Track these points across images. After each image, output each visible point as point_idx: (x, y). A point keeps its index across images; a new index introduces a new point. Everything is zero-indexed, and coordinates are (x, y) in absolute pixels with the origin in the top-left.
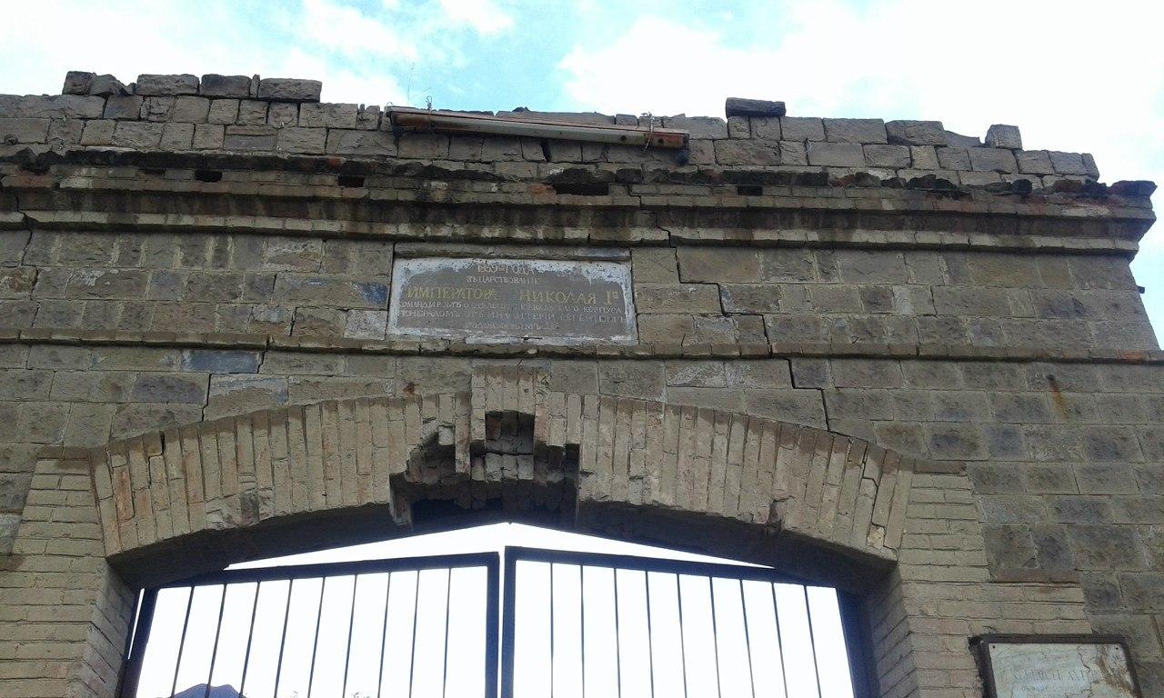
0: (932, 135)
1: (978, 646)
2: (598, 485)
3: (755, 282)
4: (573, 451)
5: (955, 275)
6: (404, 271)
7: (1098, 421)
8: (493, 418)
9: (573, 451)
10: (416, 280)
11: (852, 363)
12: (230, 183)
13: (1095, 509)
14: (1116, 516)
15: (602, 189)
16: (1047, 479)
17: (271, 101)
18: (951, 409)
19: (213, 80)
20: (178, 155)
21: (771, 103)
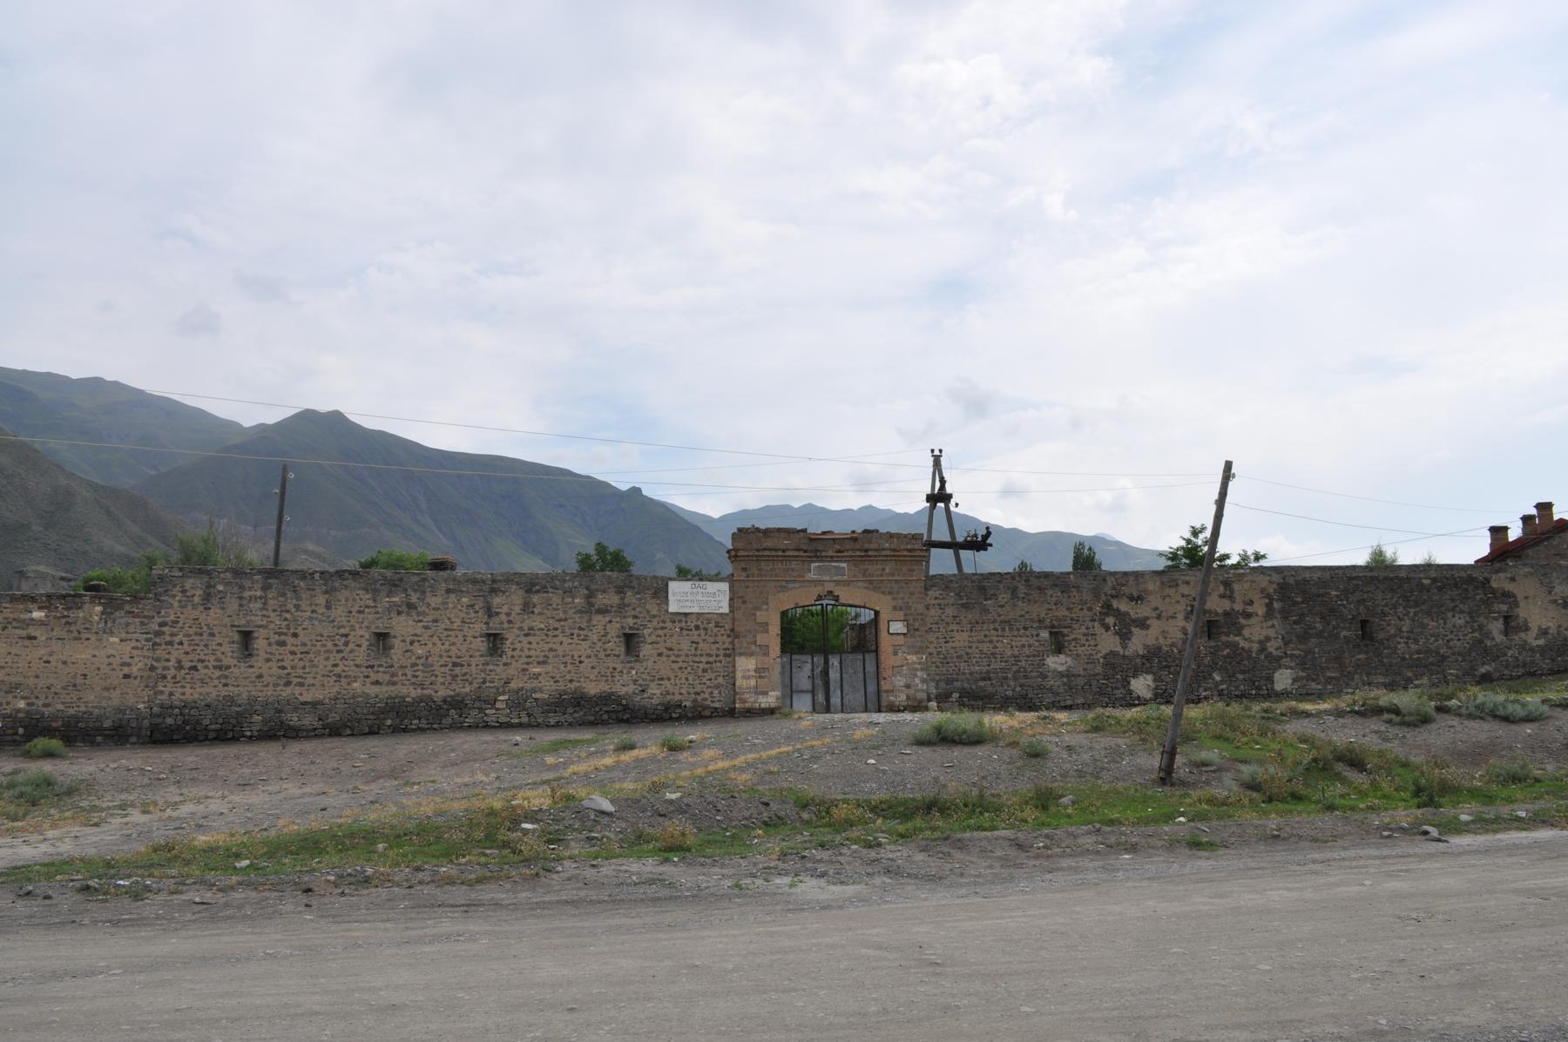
0: (788, 508)
1: (888, 622)
2: (842, 601)
3: (866, 567)
4: (838, 596)
5: (896, 565)
6: (813, 565)
7: (912, 589)
8: (828, 592)
9: (838, 596)
10: (815, 567)
11: (867, 683)
12: (787, 553)
13: (908, 603)
14: (911, 604)
15: (843, 552)
16: (902, 598)
17: (789, 533)
18: (891, 588)
19: (779, 529)
20: (1008, 529)
21: (141, 392)
